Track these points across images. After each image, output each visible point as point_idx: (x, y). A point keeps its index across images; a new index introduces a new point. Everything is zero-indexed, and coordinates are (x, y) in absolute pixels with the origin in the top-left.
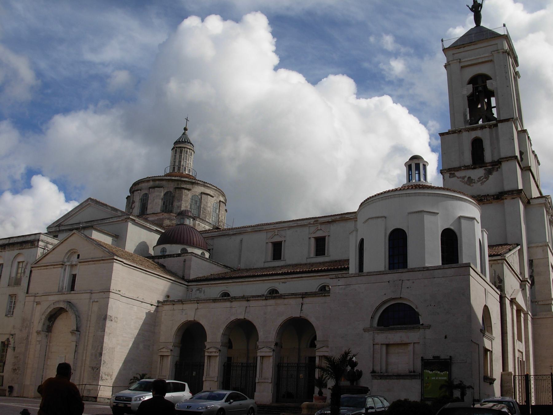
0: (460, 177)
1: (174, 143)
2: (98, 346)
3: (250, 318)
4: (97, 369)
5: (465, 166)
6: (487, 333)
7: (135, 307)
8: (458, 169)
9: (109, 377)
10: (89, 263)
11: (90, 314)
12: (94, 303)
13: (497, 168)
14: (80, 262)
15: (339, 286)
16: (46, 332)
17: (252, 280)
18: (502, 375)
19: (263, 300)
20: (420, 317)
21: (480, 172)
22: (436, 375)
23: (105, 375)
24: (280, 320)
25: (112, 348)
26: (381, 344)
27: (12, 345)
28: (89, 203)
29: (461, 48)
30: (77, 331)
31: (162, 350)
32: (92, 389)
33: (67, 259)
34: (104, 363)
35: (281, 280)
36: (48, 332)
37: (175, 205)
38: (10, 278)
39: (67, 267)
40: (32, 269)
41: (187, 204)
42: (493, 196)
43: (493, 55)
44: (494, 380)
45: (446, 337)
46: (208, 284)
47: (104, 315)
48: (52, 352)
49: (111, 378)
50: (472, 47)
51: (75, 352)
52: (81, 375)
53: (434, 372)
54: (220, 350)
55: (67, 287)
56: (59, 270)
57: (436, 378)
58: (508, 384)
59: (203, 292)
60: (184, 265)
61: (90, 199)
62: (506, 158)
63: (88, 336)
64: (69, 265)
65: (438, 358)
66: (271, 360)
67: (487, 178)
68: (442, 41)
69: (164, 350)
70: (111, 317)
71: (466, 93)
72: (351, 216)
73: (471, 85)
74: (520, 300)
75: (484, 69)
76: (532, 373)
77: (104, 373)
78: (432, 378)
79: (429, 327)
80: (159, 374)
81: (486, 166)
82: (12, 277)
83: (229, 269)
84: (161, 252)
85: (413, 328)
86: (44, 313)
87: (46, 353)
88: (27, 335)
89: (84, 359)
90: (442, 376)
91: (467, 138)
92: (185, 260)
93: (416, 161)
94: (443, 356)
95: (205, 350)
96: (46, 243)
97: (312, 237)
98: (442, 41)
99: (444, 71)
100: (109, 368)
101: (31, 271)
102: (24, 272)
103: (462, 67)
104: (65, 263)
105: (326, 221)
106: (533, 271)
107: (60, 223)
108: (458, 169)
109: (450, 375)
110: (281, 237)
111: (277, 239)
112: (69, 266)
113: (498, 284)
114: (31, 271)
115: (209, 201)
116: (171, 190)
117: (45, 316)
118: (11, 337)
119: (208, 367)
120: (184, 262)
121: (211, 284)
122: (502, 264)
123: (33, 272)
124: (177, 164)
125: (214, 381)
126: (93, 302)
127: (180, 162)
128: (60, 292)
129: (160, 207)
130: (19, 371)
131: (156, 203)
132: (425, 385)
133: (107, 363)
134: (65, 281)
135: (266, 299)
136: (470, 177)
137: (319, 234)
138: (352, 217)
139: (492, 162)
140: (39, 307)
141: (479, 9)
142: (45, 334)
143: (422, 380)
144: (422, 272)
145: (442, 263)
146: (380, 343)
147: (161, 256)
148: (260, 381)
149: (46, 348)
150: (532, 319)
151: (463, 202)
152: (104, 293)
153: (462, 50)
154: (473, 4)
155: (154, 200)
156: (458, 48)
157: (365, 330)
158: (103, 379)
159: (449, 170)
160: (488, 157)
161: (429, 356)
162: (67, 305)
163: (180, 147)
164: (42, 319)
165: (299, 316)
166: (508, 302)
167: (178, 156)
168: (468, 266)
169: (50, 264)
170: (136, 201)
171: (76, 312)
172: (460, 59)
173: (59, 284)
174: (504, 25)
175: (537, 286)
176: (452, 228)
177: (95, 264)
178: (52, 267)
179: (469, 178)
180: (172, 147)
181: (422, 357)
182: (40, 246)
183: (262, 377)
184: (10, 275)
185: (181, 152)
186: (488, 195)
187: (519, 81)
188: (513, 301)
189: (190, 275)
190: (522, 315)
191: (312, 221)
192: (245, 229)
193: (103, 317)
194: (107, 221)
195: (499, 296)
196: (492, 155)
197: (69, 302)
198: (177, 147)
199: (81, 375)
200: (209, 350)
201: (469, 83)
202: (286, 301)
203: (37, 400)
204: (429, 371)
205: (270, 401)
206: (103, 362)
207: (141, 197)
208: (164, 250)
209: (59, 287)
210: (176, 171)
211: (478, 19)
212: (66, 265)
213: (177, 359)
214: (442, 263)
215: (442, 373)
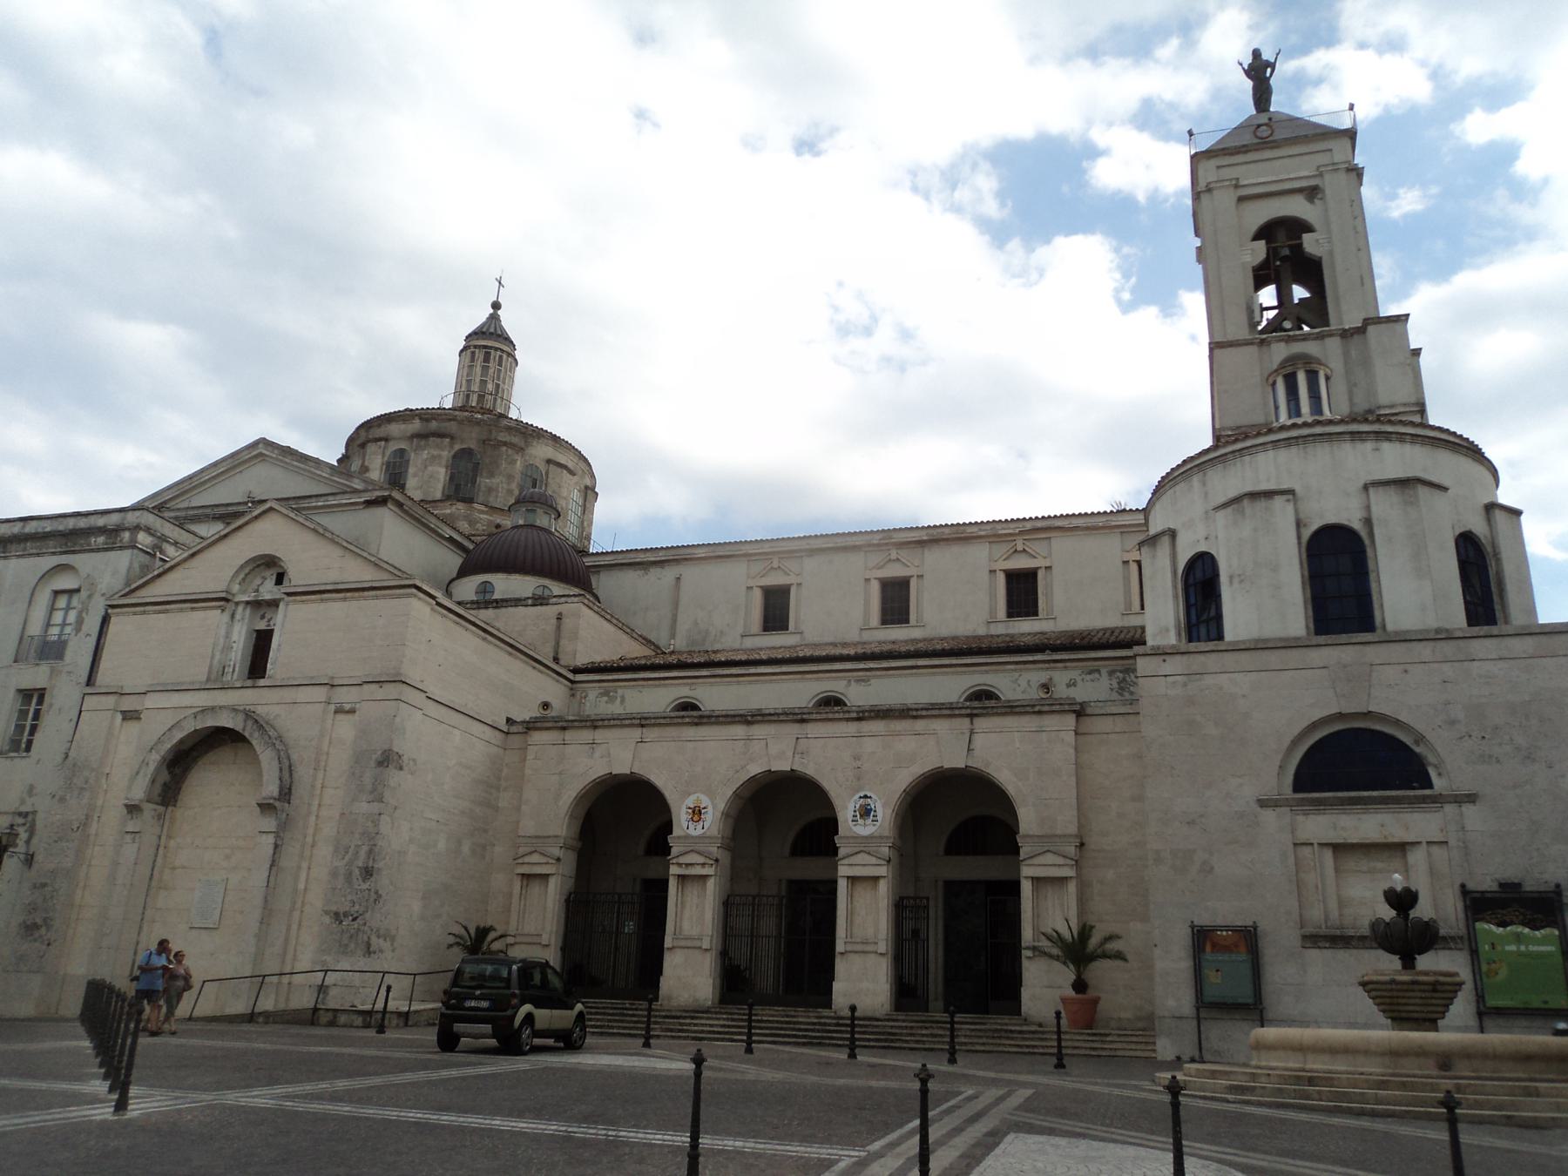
1: (467, 337)
2: (357, 846)
3: (809, 769)
4: (354, 919)
7: (457, 732)
9: (389, 943)
11: (325, 748)
12: (340, 717)
14: (289, 594)
15: (1166, 676)
16: (157, 804)
19: (848, 720)
22: (1518, 938)
23: (379, 937)
24: (905, 778)
25: (399, 852)
26: (1428, 842)
27: (21, 847)
28: (259, 451)
31: (526, 859)
32: (335, 985)
33: (240, 584)
34: (376, 900)
35: (855, 674)
36: (162, 804)
37: (483, 485)
38: (21, 638)
39: (240, 609)
46: (635, 680)
47: (380, 752)
48: (174, 868)
49: (392, 945)
50: (1268, 154)
51: (272, 866)
52: (287, 940)
53: (1509, 928)
54: (717, 860)
55: (237, 669)
56: (214, 618)
57: (1518, 948)
59: (619, 699)
60: (559, 628)
61: (263, 442)
63: (317, 816)
64: (248, 603)
66: (883, 887)
69: (535, 858)
70: (400, 756)
71: (1249, 260)
72: (980, 530)
73: (1263, 242)
75: (1296, 207)
77: (375, 930)
78: (1508, 948)
79: (1471, 798)
80: (517, 930)
82: (32, 637)
83: (652, 647)
84: (476, 593)
86: (156, 744)
87: (153, 870)
88: (87, 815)
89: (301, 886)
92: (560, 614)
95: (670, 859)
96: (159, 538)
97: (876, 579)
100: (389, 914)
101: (105, 620)
102: (80, 622)
103: (1241, 199)
105: (914, 539)
107: (165, 502)
110: (789, 575)
112: (244, 609)
114: (105, 620)
115: (566, 482)
116: (472, 446)
117: (162, 753)
118: (20, 820)
119: (679, 909)
120: (558, 618)
121: (644, 679)
125: (700, 948)
126: (336, 712)
128: (215, 681)
129: (440, 486)
132: (1484, 968)
133: (385, 900)
138: (983, 533)
140: (133, 727)
142: (155, 810)
144: (1431, 644)
146: (1424, 841)
147: (477, 602)
148: (849, 948)
149: (156, 856)
152: (381, 687)
154: (1250, 61)
155: (426, 467)
157: (1263, 803)
158: (371, 949)
161: (1485, 881)
162: (245, 721)
164: (147, 764)
165: (964, 766)
170: (371, 467)
171: (277, 743)
172: (1238, 179)
173: (213, 657)
174: (1351, 107)
177: (345, 599)
180: (462, 347)
181: (1463, 886)
182: (140, 546)
183: (851, 937)
184: (24, 628)
185: (487, 359)
192: (689, 551)
193: (374, 757)
194: (320, 504)
197: (249, 715)
198: (475, 347)
199: (287, 940)
200: (682, 860)
201: (1256, 237)
202: (920, 725)
204: (1493, 927)
205: (883, 1006)
206: (375, 897)
207: (386, 459)
208: (488, 589)
209: (211, 667)
213: (570, 883)
215: (1537, 932)
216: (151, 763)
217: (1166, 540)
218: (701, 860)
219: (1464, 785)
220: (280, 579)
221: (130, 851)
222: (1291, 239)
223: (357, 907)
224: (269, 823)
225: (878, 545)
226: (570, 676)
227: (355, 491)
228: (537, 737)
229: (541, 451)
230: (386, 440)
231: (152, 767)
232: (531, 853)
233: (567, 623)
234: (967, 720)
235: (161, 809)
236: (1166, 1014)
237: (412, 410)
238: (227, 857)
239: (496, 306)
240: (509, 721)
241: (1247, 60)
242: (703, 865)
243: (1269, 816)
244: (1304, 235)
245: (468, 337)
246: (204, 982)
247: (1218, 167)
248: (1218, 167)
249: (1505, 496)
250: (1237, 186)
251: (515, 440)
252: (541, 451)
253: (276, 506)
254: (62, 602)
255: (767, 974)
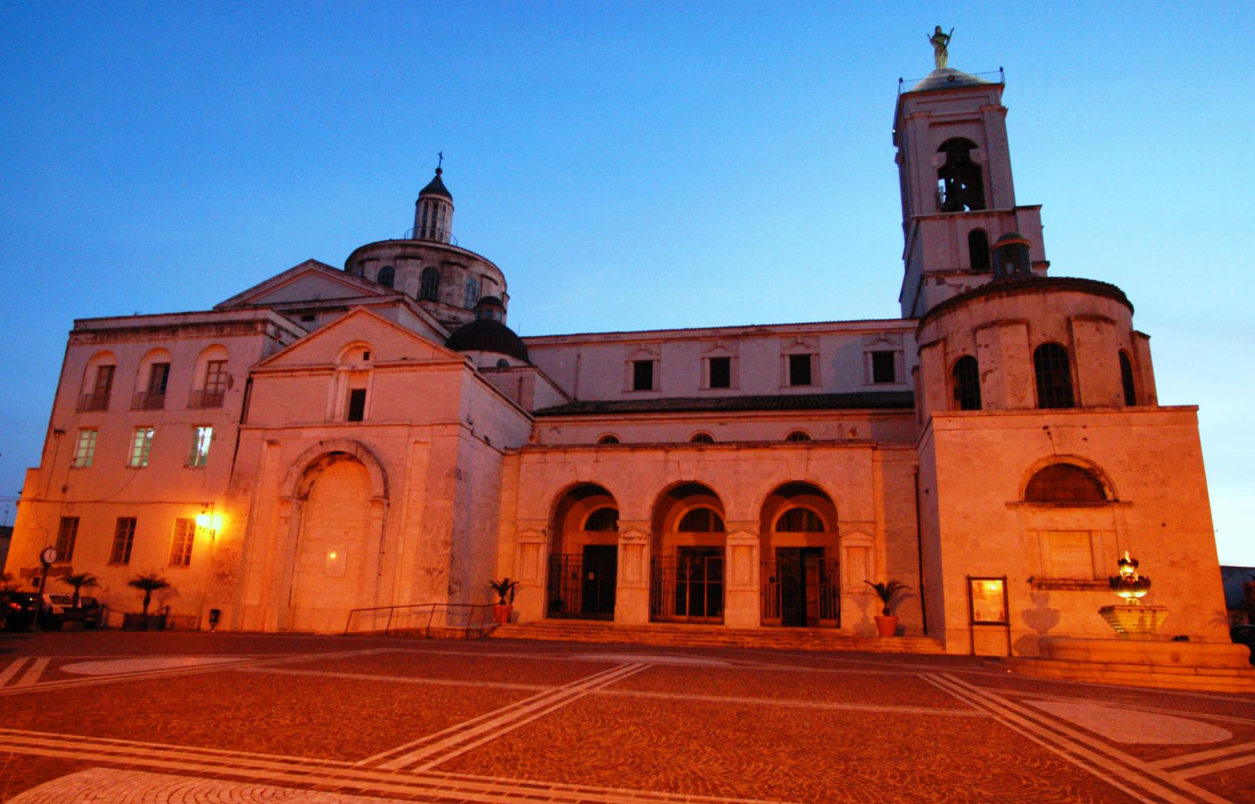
4: (441, 572)
10: (402, 369)
12: (417, 446)
17: (663, 417)
19: (730, 450)
30: (384, 498)
40: (253, 376)
41: (463, 291)
43: (982, 112)
60: (520, 387)
61: (312, 261)
64: (346, 371)
69: (530, 534)
98: (901, 80)
101: (250, 381)
104: (337, 366)
111: (644, 357)
114: (250, 381)
116: (436, 266)
123: (255, 381)
124: (429, 224)
127: (434, 223)
130: (233, 578)
131: (409, 285)
134: (339, 399)
135: (737, 449)
137: (719, 353)
140: (276, 451)
162: (357, 448)
163: (434, 199)
164: (292, 474)
167: (430, 214)
169: (301, 367)
177: (415, 371)
178: (307, 373)
185: (436, 206)
189: (532, 404)
191: (708, 333)
193: (445, 472)
200: (628, 535)
201: (941, 149)
202: (776, 453)
210: (427, 236)
212: (340, 372)
216: (294, 474)
217: (940, 346)
218: (639, 535)
220: (366, 356)
221: (285, 529)
223: (441, 565)
224: (377, 512)
225: (711, 337)
226: (533, 418)
227: (379, 296)
228: (528, 458)
229: (479, 269)
230: (377, 259)
231: (295, 476)
232: (527, 530)
233: (526, 384)
234: (806, 452)
235: (300, 502)
236: (953, 628)
237: (394, 241)
238: (346, 533)
239: (439, 171)
240: (506, 448)
242: (640, 538)
243: (1012, 514)
245: (422, 193)
246: (352, 611)
247: (918, 103)
248: (918, 103)
249: (1137, 326)
250: (929, 117)
251: (463, 261)
252: (479, 269)
253: (364, 309)
254: (215, 368)
255: (573, 599)
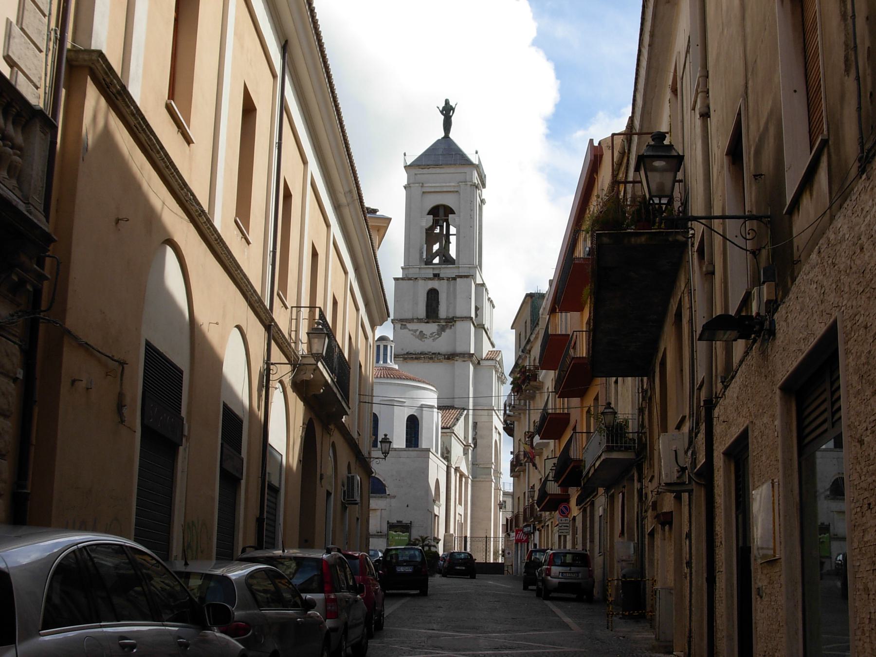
0: (412, 330)
5: (418, 319)
6: (437, 502)
8: (411, 321)
13: (451, 326)
18: (445, 536)
20: (387, 488)
21: (432, 327)
22: (399, 535)
29: (425, 168)
42: (445, 355)
44: (440, 540)
45: (408, 506)
50: (438, 170)
58: (450, 544)
62: (461, 318)
65: (401, 522)
67: (439, 335)
68: (405, 155)
73: (432, 216)
74: (464, 469)
76: (468, 535)
79: (394, 497)
81: (440, 322)
85: (382, 497)
90: (404, 536)
91: (423, 288)
93: (385, 343)
94: (405, 521)
98: (405, 155)
99: (403, 192)
103: (424, 193)
106: (476, 432)
108: (411, 321)
109: (410, 536)
113: (445, 455)
122: (451, 436)
136: (422, 331)
139: (446, 319)
141: (450, 113)
143: (388, 539)
145: (406, 445)
150: (472, 481)
151: (426, 391)
153: (425, 171)
156: (422, 169)
159: (401, 320)
160: (443, 312)
166: (453, 471)
168: (428, 450)
172: (423, 184)
174: (477, 153)
175: (479, 449)
176: (415, 414)
179: (421, 332)
186: (439, 354)
187: (484, 207)
188: (457, 469)
190: (464, 479)
195: (446, 467)
196: (447, 311)
201: (429, 214)
203: (636, 505)
211: (447, 125)
214: (407, 447)
219: (392, 494)
222: (445, 216)
241: (442, 105)
244: (450, 215)
